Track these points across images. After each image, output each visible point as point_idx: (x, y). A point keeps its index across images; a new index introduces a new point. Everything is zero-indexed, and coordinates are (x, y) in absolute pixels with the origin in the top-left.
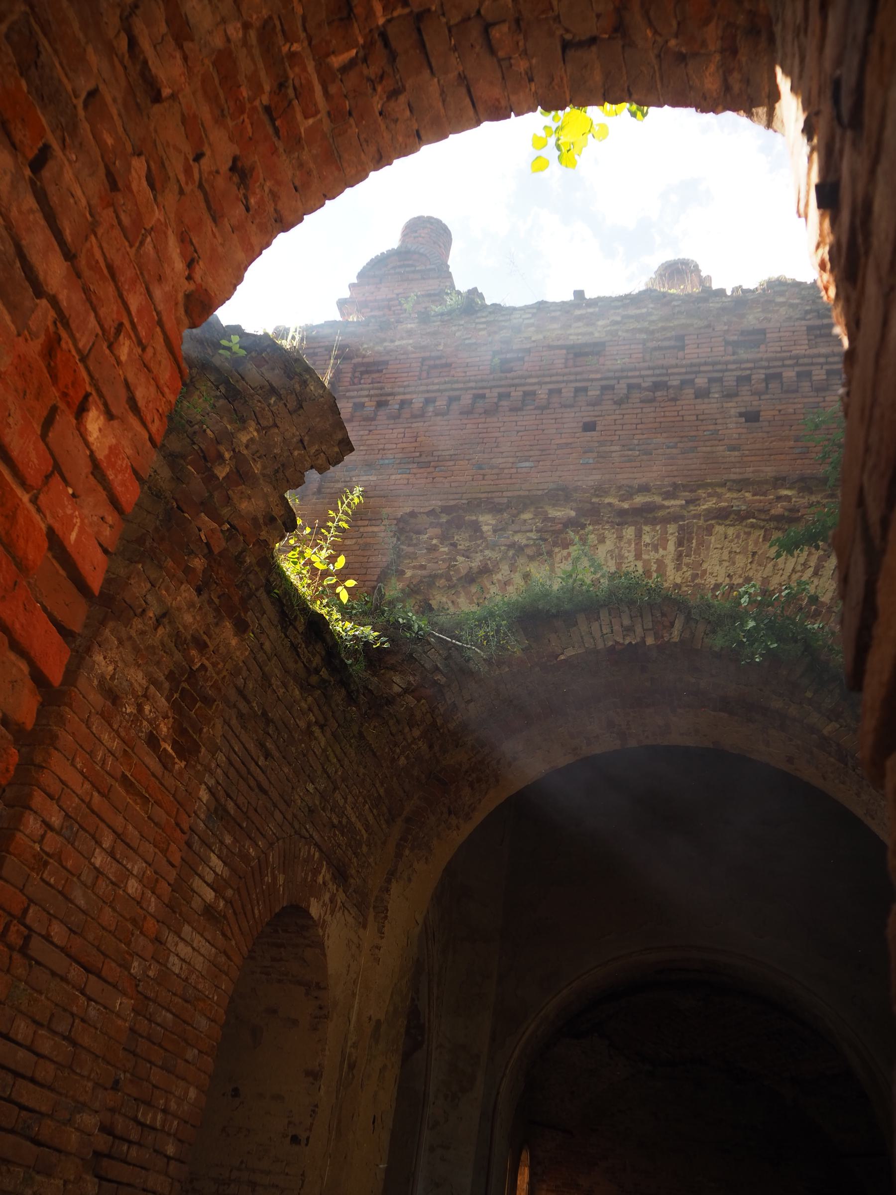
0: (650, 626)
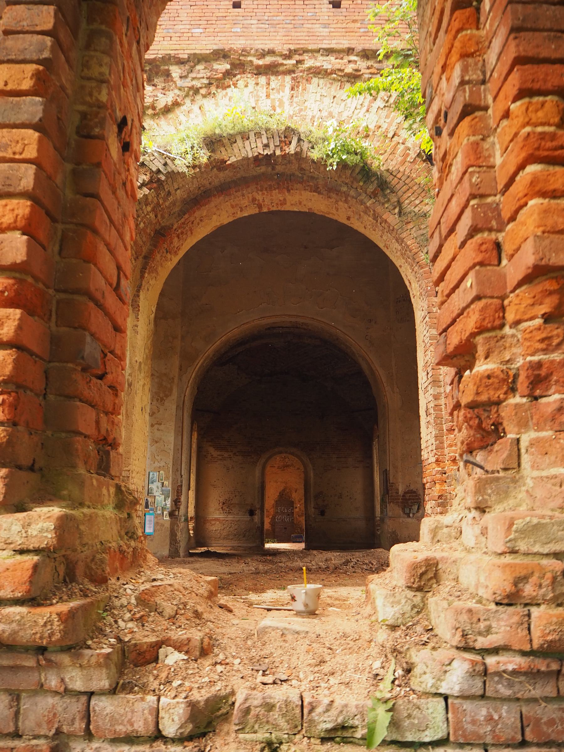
0: (278, 144)
